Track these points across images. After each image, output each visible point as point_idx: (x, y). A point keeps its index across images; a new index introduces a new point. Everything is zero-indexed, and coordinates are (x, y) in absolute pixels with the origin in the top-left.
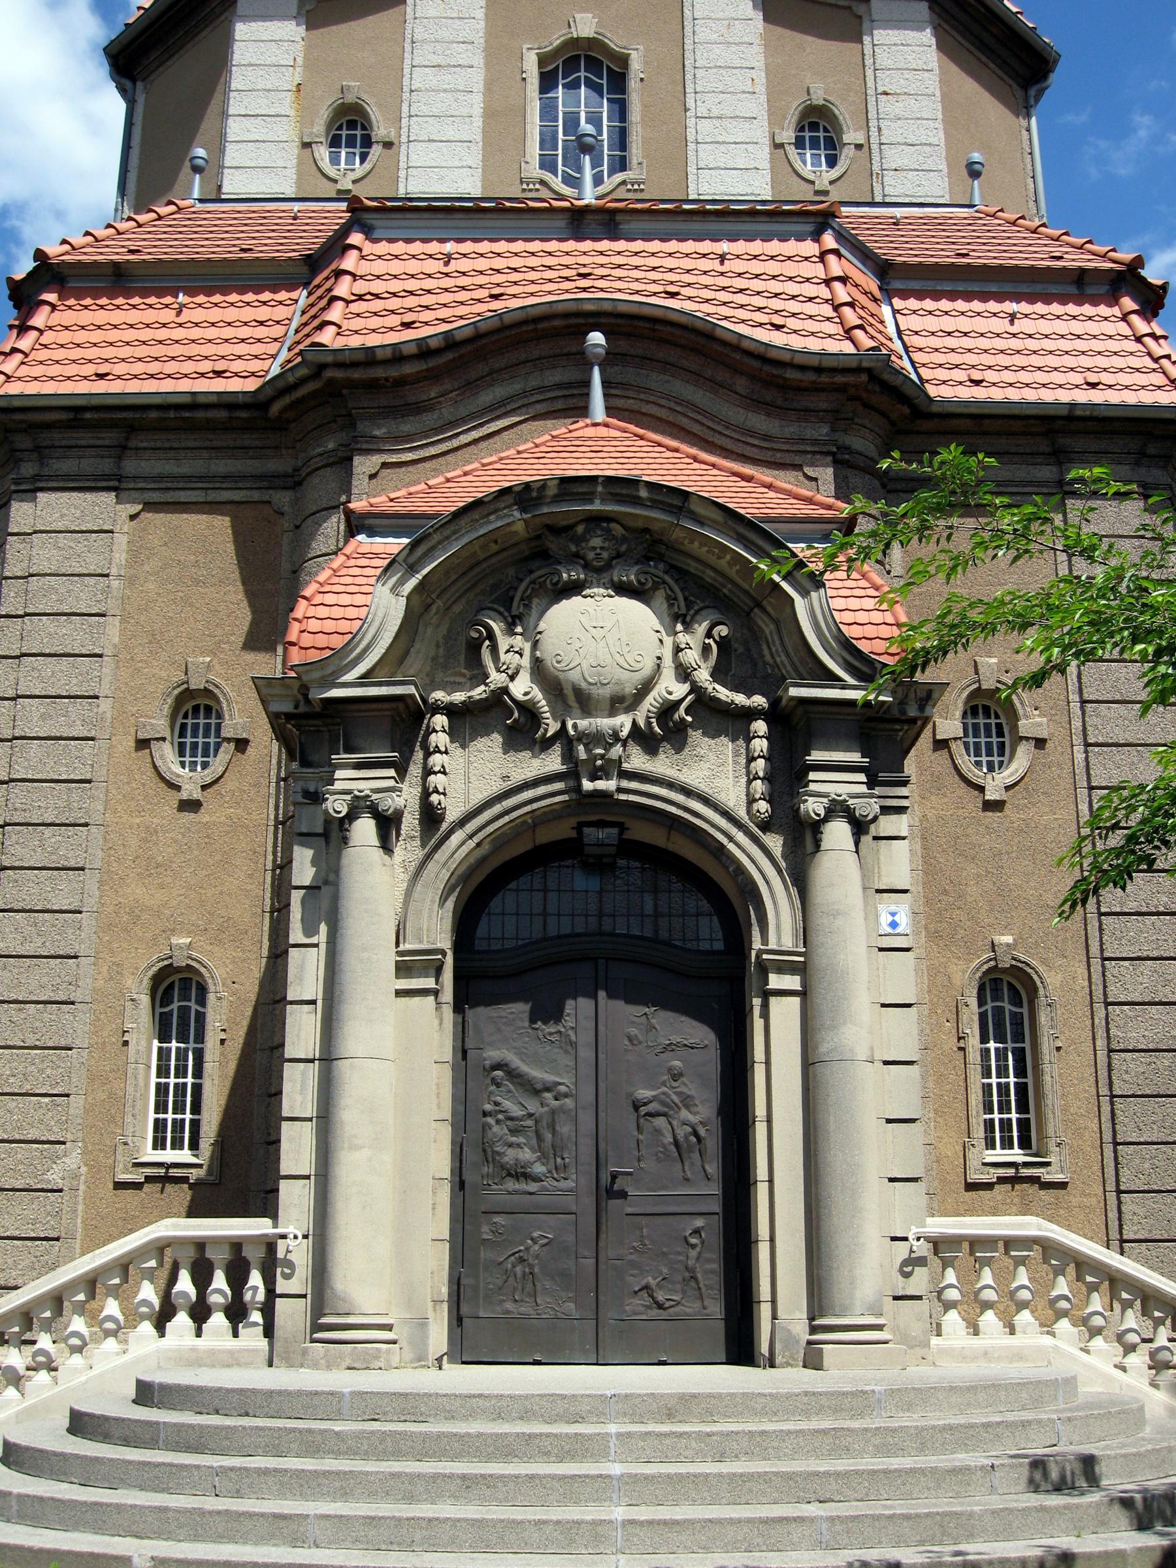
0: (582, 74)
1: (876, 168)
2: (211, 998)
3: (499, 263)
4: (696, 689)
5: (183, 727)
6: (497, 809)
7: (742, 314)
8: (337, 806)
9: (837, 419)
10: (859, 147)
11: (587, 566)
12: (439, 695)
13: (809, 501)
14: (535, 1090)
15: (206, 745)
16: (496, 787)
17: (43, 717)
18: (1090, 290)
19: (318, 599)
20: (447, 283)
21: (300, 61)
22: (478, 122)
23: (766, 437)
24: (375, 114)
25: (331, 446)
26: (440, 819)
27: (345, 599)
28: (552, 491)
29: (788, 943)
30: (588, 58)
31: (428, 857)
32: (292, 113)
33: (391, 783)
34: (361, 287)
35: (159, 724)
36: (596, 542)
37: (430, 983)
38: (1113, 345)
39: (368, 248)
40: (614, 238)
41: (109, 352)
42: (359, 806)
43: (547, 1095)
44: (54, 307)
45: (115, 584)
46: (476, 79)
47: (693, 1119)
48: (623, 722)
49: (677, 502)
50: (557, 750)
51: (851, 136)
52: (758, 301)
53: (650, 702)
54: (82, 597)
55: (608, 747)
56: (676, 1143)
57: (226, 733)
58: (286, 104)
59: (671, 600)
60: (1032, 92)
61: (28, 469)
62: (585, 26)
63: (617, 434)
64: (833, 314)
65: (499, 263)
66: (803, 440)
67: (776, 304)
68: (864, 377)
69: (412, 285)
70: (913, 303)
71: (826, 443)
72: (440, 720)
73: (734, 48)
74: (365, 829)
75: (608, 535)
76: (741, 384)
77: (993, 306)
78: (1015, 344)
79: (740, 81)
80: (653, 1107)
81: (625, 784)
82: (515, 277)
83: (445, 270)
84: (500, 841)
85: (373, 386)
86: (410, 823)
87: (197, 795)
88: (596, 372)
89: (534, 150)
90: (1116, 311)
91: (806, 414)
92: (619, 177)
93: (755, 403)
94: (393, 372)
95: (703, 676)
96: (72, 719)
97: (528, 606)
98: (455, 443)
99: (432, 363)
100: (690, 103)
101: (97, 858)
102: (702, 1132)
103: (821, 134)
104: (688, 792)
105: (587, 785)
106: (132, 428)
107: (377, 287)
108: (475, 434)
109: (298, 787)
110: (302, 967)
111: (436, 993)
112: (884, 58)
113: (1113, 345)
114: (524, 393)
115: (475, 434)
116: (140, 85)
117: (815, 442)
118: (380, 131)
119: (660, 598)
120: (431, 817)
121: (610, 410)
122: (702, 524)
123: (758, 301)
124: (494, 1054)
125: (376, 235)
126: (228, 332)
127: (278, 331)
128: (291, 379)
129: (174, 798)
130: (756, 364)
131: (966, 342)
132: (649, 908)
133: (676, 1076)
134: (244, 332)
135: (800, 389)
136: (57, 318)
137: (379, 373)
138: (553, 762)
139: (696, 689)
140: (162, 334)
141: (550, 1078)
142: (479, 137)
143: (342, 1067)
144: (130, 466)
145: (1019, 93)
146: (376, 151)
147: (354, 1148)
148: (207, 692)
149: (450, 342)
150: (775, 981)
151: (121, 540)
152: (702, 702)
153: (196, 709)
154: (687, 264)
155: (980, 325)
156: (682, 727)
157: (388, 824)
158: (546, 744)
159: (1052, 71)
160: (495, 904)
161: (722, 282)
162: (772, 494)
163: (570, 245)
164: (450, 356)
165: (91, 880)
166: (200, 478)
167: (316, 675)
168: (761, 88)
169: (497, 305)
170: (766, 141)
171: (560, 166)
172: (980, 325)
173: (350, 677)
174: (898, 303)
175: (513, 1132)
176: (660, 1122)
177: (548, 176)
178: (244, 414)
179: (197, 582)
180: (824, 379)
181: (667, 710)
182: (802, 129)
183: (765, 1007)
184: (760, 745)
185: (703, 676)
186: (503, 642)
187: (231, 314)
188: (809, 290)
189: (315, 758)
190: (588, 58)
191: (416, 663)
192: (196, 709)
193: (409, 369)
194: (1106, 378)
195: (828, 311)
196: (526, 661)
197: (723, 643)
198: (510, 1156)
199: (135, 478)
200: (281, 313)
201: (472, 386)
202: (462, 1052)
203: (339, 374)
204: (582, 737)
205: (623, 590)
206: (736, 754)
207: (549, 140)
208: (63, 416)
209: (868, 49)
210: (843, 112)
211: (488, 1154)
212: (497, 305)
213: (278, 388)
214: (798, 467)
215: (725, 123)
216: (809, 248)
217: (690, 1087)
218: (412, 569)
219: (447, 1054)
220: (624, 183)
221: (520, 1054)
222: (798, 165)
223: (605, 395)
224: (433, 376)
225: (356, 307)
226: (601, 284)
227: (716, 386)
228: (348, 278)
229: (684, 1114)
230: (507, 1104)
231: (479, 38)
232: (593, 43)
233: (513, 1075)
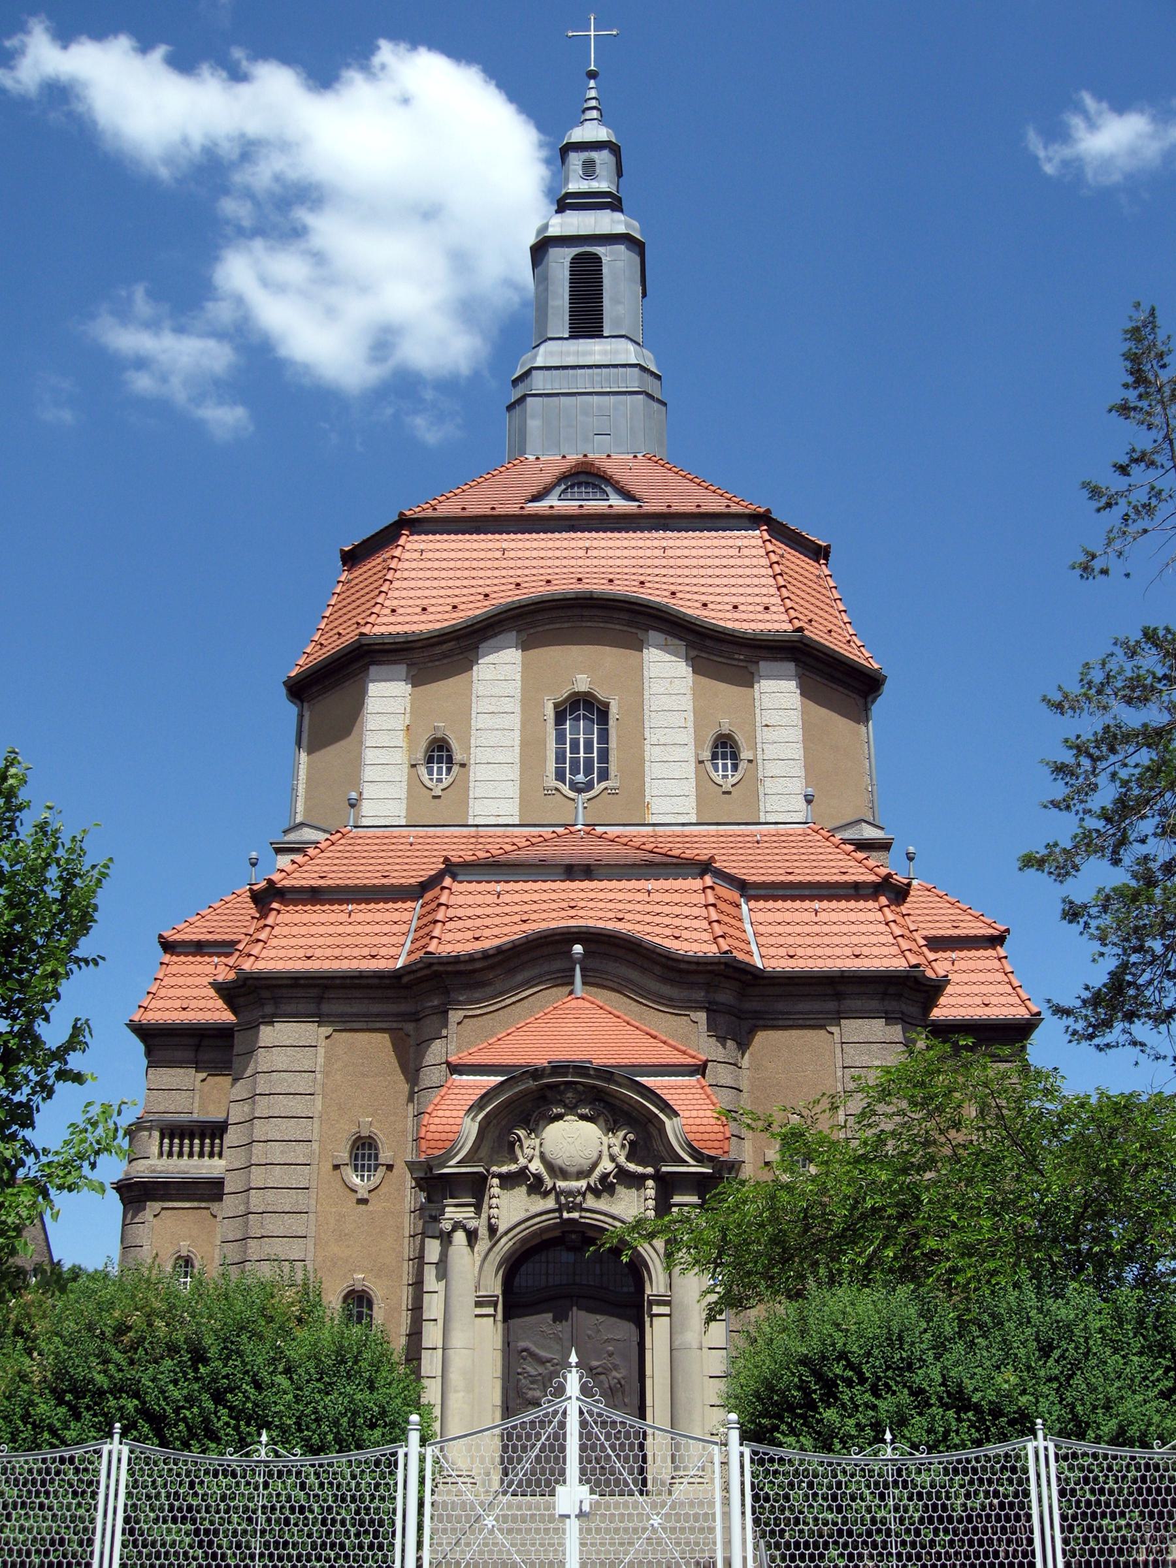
0: (582, 712)
1: (760, 776)
2: (375, 1307)
3: (526, 897)
4: (618, 1166)
5: (356, 1155)
6: (523, 1226)
7: (658, 930)
8: (446, 1226)
9: (708, 987)
10: (750, 761)
11: (565, 1106)
12: (494, 1169)
13: (684, 1053)
14: (542, 1362)
15: (369, 1165)
16: (523, 1215)
17: (282, 1152)
18: (862, 892)
19: (435, 1113)
20: (498, 910)
21: (408, 710)
22: (517, 749)
23: (671, 999)
24: (455, 745)
25: (436, 1003)
26: (497, 1230)
27: (448, 1114)
28: (548, 1071)
29: (662, 1291)
30: (586, 702)
31: (490, 1249)
32: (404, 745)
33: (472, 1215)
34: (451, 913)
35: (344, 1156)
36: (570, 1095)
37: (491, 1311)
38: (872, 928)
39: (456, 887)
40: (591, 880)
41: (311, 941)
42: (457, 1226)
43: (548, 1364)
44: (279, 912)
45: (319, 1076)
46: (515, 721)
47: (618, 1376)
48: (582, 1184)
49: (608, 1076)
50: (552, 1196)
51: (745, 755)
52: (667, 921)
53: (597, 1173)
54: (301, 1084)
55: (575, 1197)
56: (610, 1388)
57: (380, 1161)
58: (400, 739)
59: (606, 1121)
60: (870, 699)
61: (269, 1009)
62: (582, 684)
63: (588, 1005)
64: (707, 927)
65: (526, 897)
66: (690, 1001)
67: (677, 922)
68: (722, 967)
69: (479, 911)
70: (761, 904)
71: (702, 1002)
72: (496, 1181)
73: (674, 697)
74: (460, 1237)
75: (576, 1091)
76: (657, 970)
77: (807, 904)
78: (816, 929)
79: (677, 720)
80: (599, 1370)
81: (584, 1214)
82: (535, 907)
83: (498, 901)
84: (524, 1241)
85: (459, 973)
86: (483, 1232)
87: (366, 1196)
88: (578, 968)
89: (551, 766)
90: (876, 905)
91: (692, 985)
92: (603, 785)
93: (665, 980)
94: (470, 967)
95: (622, 1160)
96: (298, 1153)
97: (537, 1125)
98: (503, 1004)
99: (490, 961)
100: (647, 735)
101: (312, 1232)
102: (623, 1382)
103: (728, 750)
104: (614, 1218)
105: (566, 1215)
106: (326, 987)
107: (460, 912)
108: (514, 999)
109: (427, 1213)
110: (430, 1303)
111: (494, 1316)
112: (767, 701)
113: (872, 928)
114: (540, 976)
115: (514, 999)
116: (306, 705)
117: (696, 1001)
118: (458, 757)
119: (601, 1121)
120: (492, 1230)
121: (584, 983)
122: (620, 1086)
123: (667, 921)
124: (522, 1344)
125: (460, 878)
126: (377, 929)
127: (404, 928)
128: (414, 968)
129: (353, 1197)
130: (663, 960)
131: (789, 929)
132: (598, 1272)
133: (611, 1355)
134: (386, 928)
135: (688, 972)
136: (281, 918)
137: (462, 967)
138: (550, 1203)
139: (618, 1166)
140: (340, 929)
141: (550, 1356)
142: (518, 760)
143: (451, 1352)
144: (326, 1008)
145: (861, 701)
146: (455, 769)
147: (456, 1391)
148: (370, 1137)
149: (499, 950)
150: (656, 1310)
151: (321, 1051)
152: (623, 1174)
153: (363, 1144)
154: (629, 896)
155: (797, 916)
156: (612, 1185)
157: (472, 1236)
158: (546, 1194)
159: (883, 684)
160: (523, 1268)
161: (649, 908)
162: (666, 1048)
163: (568, 885)
164: (500, 957)
165: (310, 1242)
166: (364, 1016)
167: (436, 1162)
168: (690, 724)
169: (525, 927)
170: (693, 759)
171: (568, 775)
172: (797, 916)
173: (452, 1163)
174: (752, 904)
175: (532, 1383)
176: (602, 1377)
177: (560, 785)
178: (387, 981)
179: (363, 1075)
180: (701, 968)
181: (604, 1177)
182: (716, 747)
183: (651, 1321)
184: (651, 1193)
185: (622, 1160)
186: (526, 1143)
187: (378, 917)
188: (696, 911)
189: (435, 1198)
190: (586, 702)
191: (483, 1152)
192: (363, 1144)
193: (478, 965)
194: (865, 950)
195: (705, 924)
196: (537, 1153)
197: (631, 1143)
198: (530, 1394)
199: (328, 1015)
200: (406, 916)
201: (512, 972)
202: (507, 1344)
203: (441, 968)
204: (562, 1192)
205: (583, 1117)
206: (639, 1196)
207: (560, 757)
208: (289, 982)
209: (757, 695)
210: (740, 738)
211: (520, 1394)
212: (525, 927)
213: (407, 970)
214: (822, 1027)
215: (668, 748)
216: (697, 884)
217: (617, 1360)
218: (482, 1109)
219: (499, 1345)
220: (606, 789)
221: (535, 1344)
222: (713, 774)
223: (582, 976)
224: (491, 967)
225: (449, 925)
226: (582, 913)
227: (643, 970)
228: (443, 908)
229: (615, 1373)
230: (529, 1369)
231: (518, 693)
232: (588, 694)
233: (532, 1355)
